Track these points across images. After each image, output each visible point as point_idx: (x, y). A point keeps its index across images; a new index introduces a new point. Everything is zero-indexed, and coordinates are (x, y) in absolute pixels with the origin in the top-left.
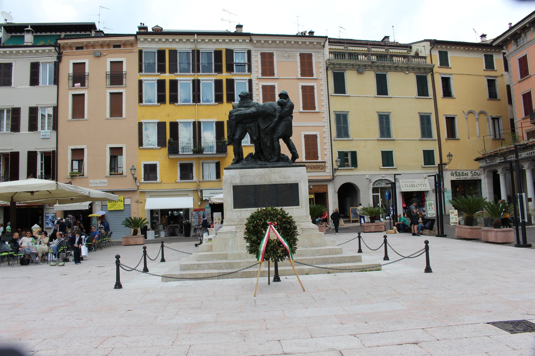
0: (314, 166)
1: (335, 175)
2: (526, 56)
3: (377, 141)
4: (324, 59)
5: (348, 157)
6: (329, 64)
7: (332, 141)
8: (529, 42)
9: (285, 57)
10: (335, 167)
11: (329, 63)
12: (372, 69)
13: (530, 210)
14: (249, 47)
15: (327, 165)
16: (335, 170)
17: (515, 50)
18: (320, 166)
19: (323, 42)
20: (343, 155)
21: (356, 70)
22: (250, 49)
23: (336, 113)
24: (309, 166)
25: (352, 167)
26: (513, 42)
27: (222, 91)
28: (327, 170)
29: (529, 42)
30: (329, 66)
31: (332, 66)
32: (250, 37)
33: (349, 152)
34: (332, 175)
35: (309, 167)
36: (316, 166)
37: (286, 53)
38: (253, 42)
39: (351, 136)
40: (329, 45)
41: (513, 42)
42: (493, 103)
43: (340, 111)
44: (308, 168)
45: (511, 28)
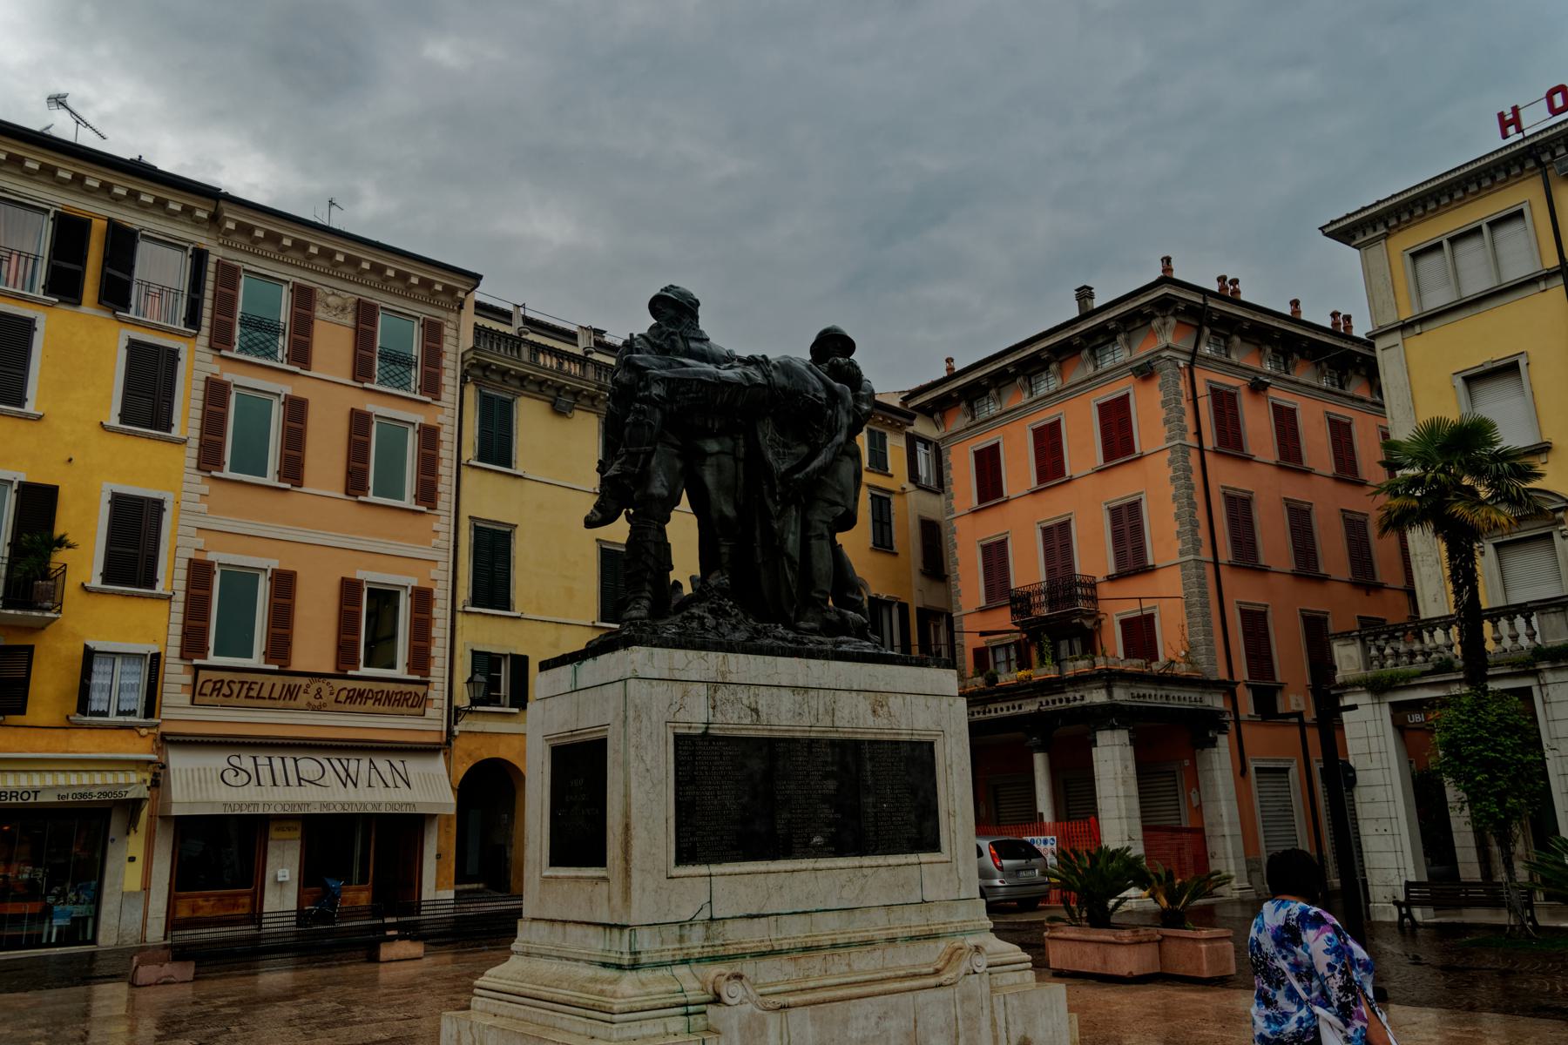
0: (290, 686)
1: (456, 729)
2: (996, 446)
3: (590, 629)
4: (457, 346)
5: (500, 672)
6: (472, 365)
7: (459, 616)
8: (1006, 413)
9: (328, 306)
10: (462, 699)
11: (474, 361)
12: (594, 406)
13: (461, 770)
14: (203, 239)
15: (432, 694)
16: (456, 716)
17: (968, 429)
18: (408, 696)
19: (463, 290)
20: (485, 663)
21: (550, 402)
22: (205, 247)
23: (479, 524)
24: (370, 690)
25: (510, 707)
26: (963, 405)
27: (82, 259)
28: (430, 712)
29: (1006, 413)
30: (471, 371)
31: (478, 373)
32: (214, 202)
33: (505, 656)
34: (445, 728)
35: (370, 695)
36: (397, 694)
37: (333, 294)
38: (220, 226)
39: (516, 604)
40: (475, 314)
41: (963, 405)
42: (882, 559)
43: (490, 521)
44: (367, 698)
45: (953, 376)
